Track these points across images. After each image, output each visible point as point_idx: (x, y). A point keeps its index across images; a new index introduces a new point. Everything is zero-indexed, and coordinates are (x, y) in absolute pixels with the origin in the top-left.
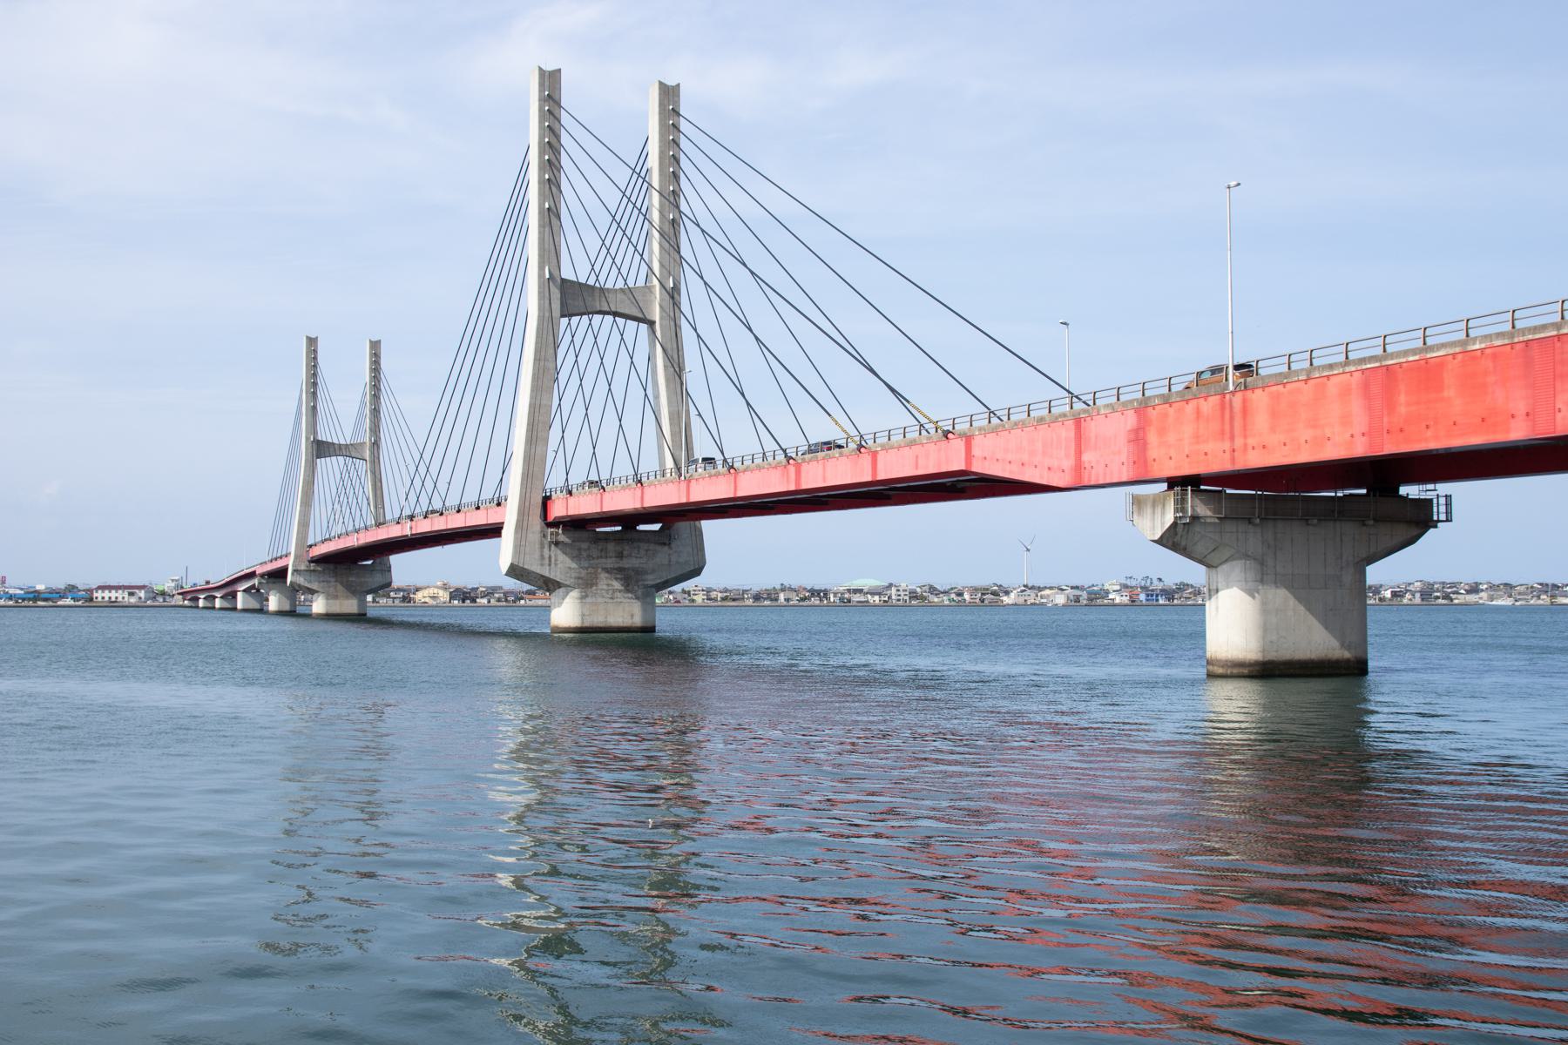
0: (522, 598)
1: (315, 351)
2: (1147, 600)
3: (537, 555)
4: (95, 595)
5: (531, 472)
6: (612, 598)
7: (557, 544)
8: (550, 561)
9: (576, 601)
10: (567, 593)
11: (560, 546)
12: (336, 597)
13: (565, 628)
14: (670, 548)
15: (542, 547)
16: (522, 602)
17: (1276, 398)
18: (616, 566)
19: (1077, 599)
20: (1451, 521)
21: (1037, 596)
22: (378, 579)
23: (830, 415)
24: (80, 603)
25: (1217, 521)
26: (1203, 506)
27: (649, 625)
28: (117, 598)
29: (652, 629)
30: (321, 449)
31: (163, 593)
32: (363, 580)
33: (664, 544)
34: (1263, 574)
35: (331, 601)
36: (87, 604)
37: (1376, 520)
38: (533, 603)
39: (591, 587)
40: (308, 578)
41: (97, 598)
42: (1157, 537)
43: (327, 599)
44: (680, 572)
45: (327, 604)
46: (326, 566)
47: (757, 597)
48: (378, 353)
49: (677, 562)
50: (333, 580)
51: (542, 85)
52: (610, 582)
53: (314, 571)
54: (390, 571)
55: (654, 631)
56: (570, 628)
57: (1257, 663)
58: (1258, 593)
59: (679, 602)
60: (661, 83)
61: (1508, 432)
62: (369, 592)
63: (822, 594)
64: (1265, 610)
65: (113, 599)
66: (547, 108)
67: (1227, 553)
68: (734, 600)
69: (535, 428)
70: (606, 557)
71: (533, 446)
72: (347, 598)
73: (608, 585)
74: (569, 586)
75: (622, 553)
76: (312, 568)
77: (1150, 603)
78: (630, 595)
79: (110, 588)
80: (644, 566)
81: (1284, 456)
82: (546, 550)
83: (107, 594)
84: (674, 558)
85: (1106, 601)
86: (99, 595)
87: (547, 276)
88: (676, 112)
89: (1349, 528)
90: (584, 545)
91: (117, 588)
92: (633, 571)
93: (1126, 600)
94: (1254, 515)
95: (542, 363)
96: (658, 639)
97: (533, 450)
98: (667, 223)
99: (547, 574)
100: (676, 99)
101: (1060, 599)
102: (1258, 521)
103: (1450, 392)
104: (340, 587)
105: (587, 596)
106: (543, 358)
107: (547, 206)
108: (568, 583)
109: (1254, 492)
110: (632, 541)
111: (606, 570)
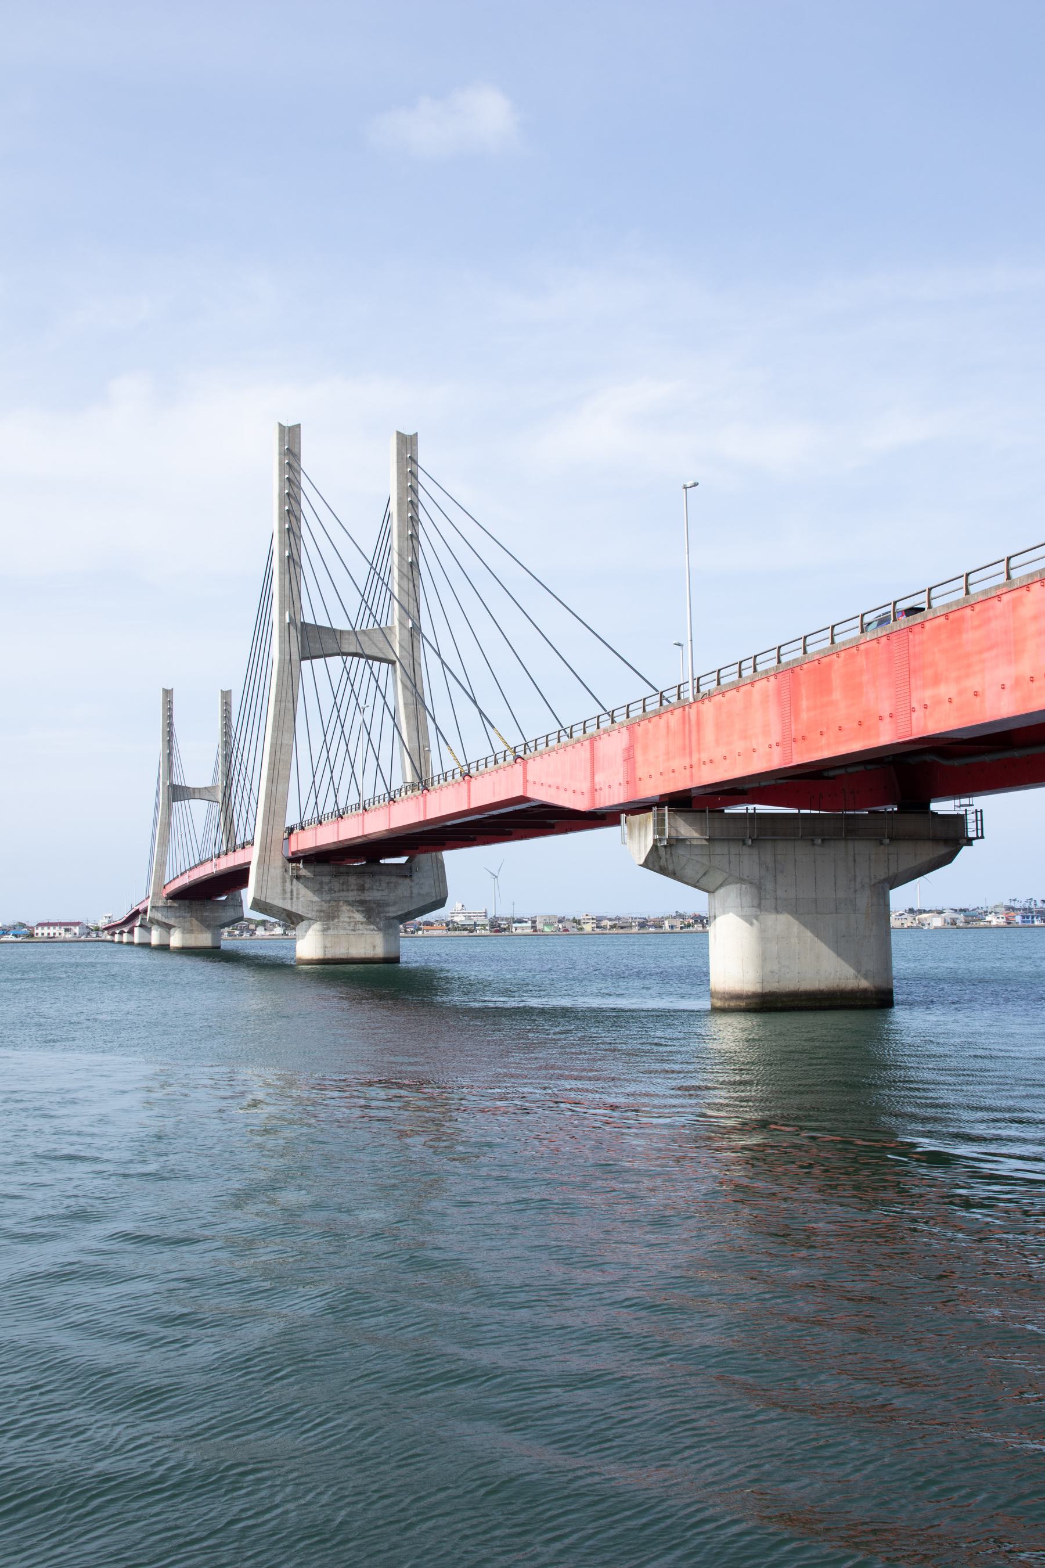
0: (420, 929)
1: (171, 702)
2: (1024, 922)
3: (279, 889)
4: (36, 931)
5: (272, 809)
6: (354, 930)
7: (298, 878)
8: (292, 895)
9: (318, 933)
10: (310, 926)
11: (301, 881)
12: (191, 931)
13: (308, 960)
14: (412, 881)
15: (284, 881)
16: (420, 932)
17: (719, 707)
18: (358, 898)
19: (954, 922)
20: (982, 837)
21: (914, 919)
22: (229, 914)
23: (447, 744)
24: (20, 939)
25: (705, 843)
26: (688, 827)
27: (392, 955)
28: (54, 934)
29: (396, 960)
30: (177, 793)
31: (97, 929)
32: (216, 914)
33: (406, 876)
34: (760, 899)
35: (187, 936)
36: (26, 940)
37: (891, 839)
38: (431, 933)
39: (333, 918)
40: (165, 913)
41: (37, 934)
42: (641, 863)
43: (183, 933)
44: (421, 904)
45: (183, 938)
46: (181, 902)
47: (642, 925)
48: (229, 702)
49: (419, 894)
50: (188, 915)
51: (281, 439)
52: (352, 915)
53: (170, 907)
54: (241, 906)
55: (398, 962)
56: (312, 960)
57: (754, 995)
58: (757, 920)
59: (567, 930)
60: (398, 433)
61: (878, 735)
62: (223, 926)
63: (705, 921)
64: (763, 938)
65: (52, 935)
66: (286, 461)
67: (719, 878)
68: (622, 928)
69: (277, 767)
70: (348, 890)
71: (275, 784)
72: (202, 931)
73: (350, 917)
74: (311, 919)
75: (363, 885)
76: (169, 905)
77: (1027, 924)
78: (372, 927)
79: (49, 925)
80: (386, 898)
81: (726, 771)
82: (288, 884)
83: (46, 930)
84: (415, 891)
85: (982, 924)
86: (39, 931)
87: (288, 621)
88: (413, 460)
89: (863, 848)
90: (326, 879)
91: (54, 925)
92: (375, 903)
93: (1002, 922)
94: (884, 836)
95: (283, 704)
96: (400, 970)
97: (274, 788)
98: (406, 564)
99: (289, 908)
100: (414, 448)
101: (937, 922)
102: (750, 842)
103: (837, 695)
104: (195, 922)
105: (328, 929)
106: (284, 699)
107: (287, 554)
108: (309, 916)
109: (796, 811)
110: (373, 874)
111: (350, 904)
